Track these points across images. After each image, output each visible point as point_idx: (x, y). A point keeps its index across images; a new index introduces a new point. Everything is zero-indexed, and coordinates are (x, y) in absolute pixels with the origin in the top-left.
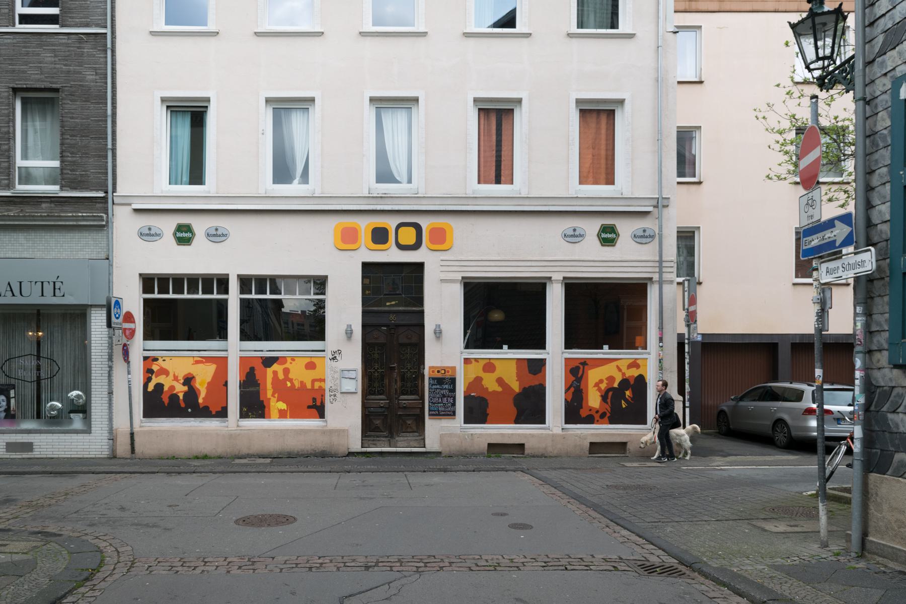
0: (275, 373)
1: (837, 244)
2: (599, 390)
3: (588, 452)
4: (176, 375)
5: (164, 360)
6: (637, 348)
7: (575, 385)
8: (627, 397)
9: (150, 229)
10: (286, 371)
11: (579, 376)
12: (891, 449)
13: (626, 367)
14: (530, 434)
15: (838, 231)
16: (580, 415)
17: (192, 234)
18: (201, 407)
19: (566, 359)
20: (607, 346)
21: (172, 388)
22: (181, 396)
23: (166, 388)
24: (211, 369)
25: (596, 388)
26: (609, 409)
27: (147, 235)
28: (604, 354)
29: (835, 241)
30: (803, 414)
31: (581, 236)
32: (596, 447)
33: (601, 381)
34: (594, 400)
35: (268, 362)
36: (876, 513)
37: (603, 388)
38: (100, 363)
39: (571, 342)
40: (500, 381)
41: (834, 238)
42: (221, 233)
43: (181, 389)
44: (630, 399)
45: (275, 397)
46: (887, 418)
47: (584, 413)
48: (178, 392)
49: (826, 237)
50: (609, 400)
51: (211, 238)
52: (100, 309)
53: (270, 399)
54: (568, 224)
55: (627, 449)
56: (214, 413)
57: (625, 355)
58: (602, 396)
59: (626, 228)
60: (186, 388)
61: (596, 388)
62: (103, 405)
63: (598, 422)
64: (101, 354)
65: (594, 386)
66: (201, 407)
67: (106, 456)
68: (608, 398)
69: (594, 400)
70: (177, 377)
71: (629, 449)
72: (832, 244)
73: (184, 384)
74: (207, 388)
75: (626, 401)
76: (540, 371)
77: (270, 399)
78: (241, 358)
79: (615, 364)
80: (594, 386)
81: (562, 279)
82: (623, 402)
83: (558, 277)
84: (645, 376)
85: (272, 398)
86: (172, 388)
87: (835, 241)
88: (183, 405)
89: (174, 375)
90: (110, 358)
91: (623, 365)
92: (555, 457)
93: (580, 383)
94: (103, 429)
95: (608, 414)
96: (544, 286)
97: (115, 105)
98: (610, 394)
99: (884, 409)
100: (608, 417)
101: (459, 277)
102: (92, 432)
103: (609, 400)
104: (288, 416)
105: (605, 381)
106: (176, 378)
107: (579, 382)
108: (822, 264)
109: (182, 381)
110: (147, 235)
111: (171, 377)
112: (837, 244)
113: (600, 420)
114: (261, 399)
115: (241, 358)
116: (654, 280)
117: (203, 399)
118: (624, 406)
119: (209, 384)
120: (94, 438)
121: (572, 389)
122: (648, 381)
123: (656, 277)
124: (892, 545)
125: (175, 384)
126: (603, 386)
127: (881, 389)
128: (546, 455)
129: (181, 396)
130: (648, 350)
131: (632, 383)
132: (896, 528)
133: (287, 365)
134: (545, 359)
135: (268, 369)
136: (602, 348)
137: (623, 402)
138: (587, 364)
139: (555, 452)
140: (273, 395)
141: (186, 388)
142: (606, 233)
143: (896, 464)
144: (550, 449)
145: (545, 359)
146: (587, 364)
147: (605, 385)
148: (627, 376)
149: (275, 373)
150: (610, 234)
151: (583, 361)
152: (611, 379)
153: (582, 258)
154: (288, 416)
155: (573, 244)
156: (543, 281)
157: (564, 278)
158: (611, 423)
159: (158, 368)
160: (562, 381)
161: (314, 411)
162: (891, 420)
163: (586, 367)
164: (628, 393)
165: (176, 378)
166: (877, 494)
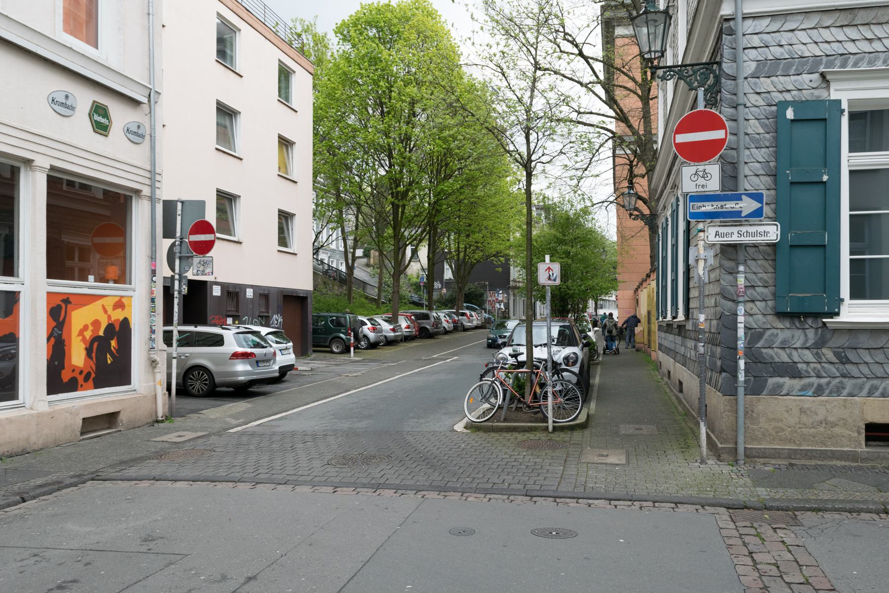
1: (743, 215)
2: (84, 340)
3: (79, 434)
6: (107, 281)
7: (56, 334)
8: (112, 348)
11: (61, 319)
13: (111, 307)
14: (7, 419)
15: (745, 205)
16: (62, 379)
17: (109, 122)
20: (93, 277)
25: (80, 338)
26: (94, 368)
27: (62, 104)
28: (90, 287)
29: (741, 212)
30: (230, 359)
31: (72, 108)
32: (91, 424)
33: (86, 327)
34: (78, 356)
36: (751, 426)
37: (88, 337)
39: (56, 269)
41: (740, 209)
44: (115, 352)
46: (762, 353)
47: (66, 376)
49: (727, 206)
50: (94, 355)
51: (130, 136)
54: (60, 85)
55: (119, 421)
57: (111, 290)
58: (86, 349)
59: (120, 115)
61: (80, 338)
63: (83, 388)
65: (78, 335)
68: (93, 352)
69: (78, 356)
71: (122, 421)
72: (738, 214)
75: (112, 354)
76: (11, 313)
78: (49, 293)
79: (100, 303)
80: (78, 335)
81: (49, 167)
82: (108, 356)
83: (43, 162)
84: (129, 319)
87: (741, 212)
91: (109, 303)
92: (41, 449)
93: (62, 331)
95: (93, 375)
96: (14, 172)
98: (96, 344)
99: (759, 345)
100: (94, 379)
103: (94, 355)
105: (91, 328)
107: (61, 329)
108: (710, 228)
112: (743, 215)
113: (84, 384)
115: (49, 293)
116: (143, 193)
118: (109, 362)
121: (53, 340)
122: (132, 326)
123: (146, 191)
124: (773, 447)
126: (88, 334)
127: (753, 330)
128: (29, 450)
130: (133, 286)
131: (117, 329)
132: (774, 434)
134: (19, 292)
136: (87, 280)
137: (108, 356)
138: (70, 302)
139: (40, 443)
142: (99, 116)
143: (771, 386)
144: (33, 439)
145: (19, 292)
146: (70, 302)
147: (91, 333)
148: (113, 319)
150: (103, 117)
151: (65, 297)
152: (96, 323)
153: (74, 143)
155: (61, 117)
156: (16, 164)
157: (53, 168)
158: (96, 386)
162: (766, 353)
163: (69, 306)
164: (113, 343)
166: (753, 411)
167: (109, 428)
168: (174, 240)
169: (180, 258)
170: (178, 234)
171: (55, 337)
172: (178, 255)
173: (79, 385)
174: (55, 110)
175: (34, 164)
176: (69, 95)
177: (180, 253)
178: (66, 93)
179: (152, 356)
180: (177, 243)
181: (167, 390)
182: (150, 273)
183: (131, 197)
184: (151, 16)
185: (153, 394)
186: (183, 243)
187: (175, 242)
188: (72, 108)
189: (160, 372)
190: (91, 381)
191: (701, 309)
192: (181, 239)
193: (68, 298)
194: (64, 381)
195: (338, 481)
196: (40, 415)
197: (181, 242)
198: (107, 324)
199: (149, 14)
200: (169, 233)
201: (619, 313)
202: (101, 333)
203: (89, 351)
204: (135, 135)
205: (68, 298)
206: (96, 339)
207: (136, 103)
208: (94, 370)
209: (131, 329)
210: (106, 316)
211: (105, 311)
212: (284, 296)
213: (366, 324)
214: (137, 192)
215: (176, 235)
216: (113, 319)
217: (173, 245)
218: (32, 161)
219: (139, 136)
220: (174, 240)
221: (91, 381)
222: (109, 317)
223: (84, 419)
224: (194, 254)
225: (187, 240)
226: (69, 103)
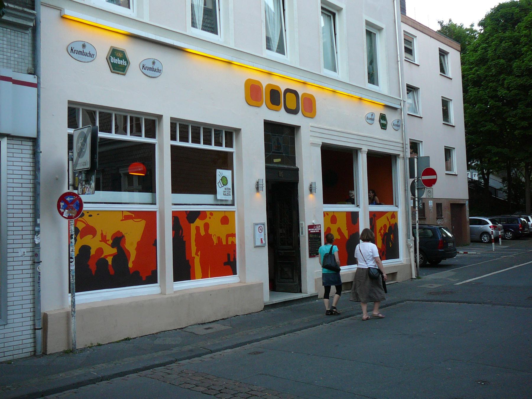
0: (198, 228)
4: (104, 234)
5: (90, 216)
9: (84, 46)
10: (207, 226)
12: (474, 146)
17: (127, 63)
18: (131, 272)
19: (370, 212)
21: (100, 251)
22: (110, 260)
23: (93, 252)
24: (140, 225)
27: (80, 53)
31: (159, 71)
35: (193, 216)
38: (20, 220)
40: (339, 230)
42: (157, 68)
43: (109, 251)
45: (198, 256)
48: (106, 256)
51: (146, 71)
52: (20, 142)
53: (194, 258)
56: (144, 279)
60: (114, 251)
62: (24, 280)
64: (22, 207)
65: (379, 233)
66: (131, 272)
67: (28, 355)
70: (105, 236)
73: (113, 246)
74: (137, 249)
77: (194, 258)
80: (379, 233)
83: (365, 149)
85: (196, 256)
86: (100, 251)
88: (112, 272)
89: (102, 234)
90: (36, 214)
94: (24, 315)
97: (269, 44)
101: (320, 142)
102: (9, 321)
104: (209, 276)
106: (104, 239)
109: (110, 242)
110: (80, 53)
111: (98, 237)
114: (187, 259)
117: (133, 262)
119: (139, 244)
120: (11, 330)
125: (103, 245)
129: (110, 260)
133: (207, 220)
135: (192, 224)
140: (197, 254)
141: (114, 251)
149: (198, 228)
152: (385, 226)
154: (209, 276)
159: (84, 225)
160: (184, 282)
161: (228, 267)
165: (104, 239)
167: (392, 280)
168: (414, 179)
169: (418, 189)
170: (416, 176)
172: (416, 187)
175: (362, 150)
176: (86, 44)
177: (418, 186)
178: (83, 43)
180: (416, 181)
181: (415, 262)
185: (410, 264)
186: (419, 180)
187: (415, 180)
188: (159, 71)
191: (72, 251)
192: (417, 178)
197: (418, 180)
200: (412, 176)
201: (433, 201)
202: (387, 231)
206: (385, 234)
207: (395, 109)
209: (398, 229)
211: (388, 220)
212: (451, 204)
213: (488, 224)
215: (415, 176)
216: (391, 224)
217: (414, 182)
219: (155, 71)
220: (414, 179)
222: (390, 223)
224: (425, 186)
225: (421, 179)
226: (155, 67)
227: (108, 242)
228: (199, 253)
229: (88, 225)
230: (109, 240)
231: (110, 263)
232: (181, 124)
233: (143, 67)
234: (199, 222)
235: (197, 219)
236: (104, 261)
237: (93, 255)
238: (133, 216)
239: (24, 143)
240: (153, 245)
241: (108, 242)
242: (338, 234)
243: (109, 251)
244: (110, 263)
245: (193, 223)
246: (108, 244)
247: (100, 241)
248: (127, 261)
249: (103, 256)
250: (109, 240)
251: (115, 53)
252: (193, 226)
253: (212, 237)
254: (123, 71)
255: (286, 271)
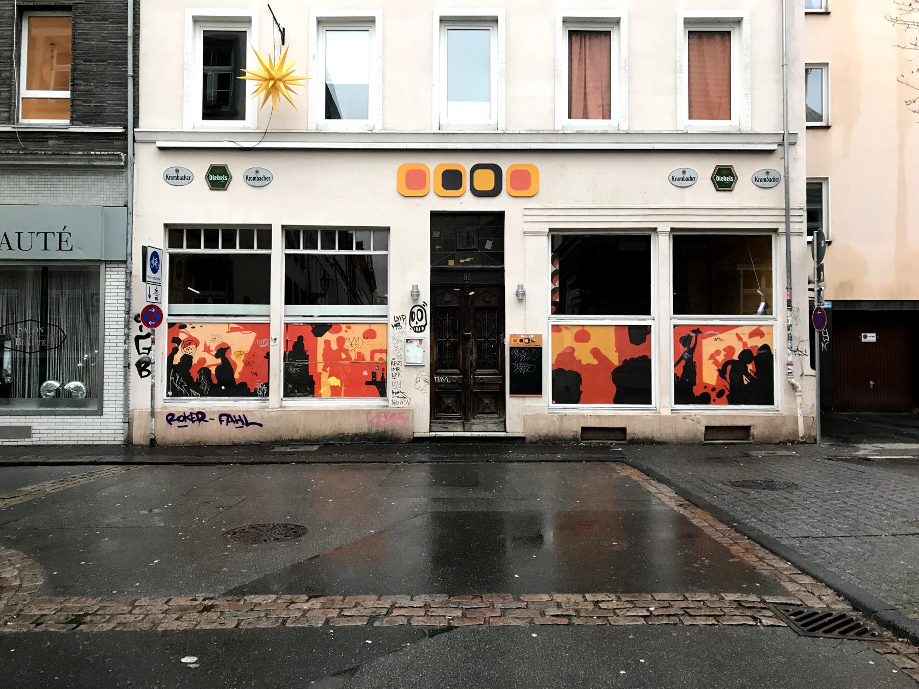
2: (716, 363)
8: (749, 371)
11: (691, 346)
16: (693, 394)
17: (228, 177)
18: (237, 383)
21: (203, 360)
22: (213, 370)
23: (195, 361)
25: (712, 361)
31: (692, 179)
33: (718, 352)
34: (709, 375)
43: (213, 362)
48: (210, 366)
50: (727, 376)
53: (321, 373)
54: (676, 165)
58: (719, 370)
60: (219, 361)
65: (710, 359)
66: (237, 383)
69: (709, 375)
70: (209, 347)
73: (217, 356)
75: (748, 376)
77: (321, 373)
82: (744, 377)
83: (664, 228)
85: (324, 373)
86: (203, 360)
89: (205, 345)
91: (745, 333)
95: (727, 393)
96: (648, 238)
98: (729, 367)
100: (727, 396)
103: (727, 376)
106: (207, 349)
111: (201, 347)
114: (310, 374)
117: (240, 373)
118: (746, 383)
120: (106, 420)
122: (774, 353)
123: (782, 228)
125: (206, 355)
126: (721, 358)
129: (213, 370)
130: (774, 315)
135: (319, 338)
137: (744, 377)
141: (219, 361)
145: (651, 326)
146: (701, 332)
148: (749, 346)
149: (327, 343)
151: (695, 328)
152: (730, 350)
155: (682, 189)
156: (647, 233)
158: (730, 403)
163: (699, 335)
164: (750, 367)
165: (207, 349)
171: (685, 360)
173: (712, 400)
174: (677, 186)
176: (259, 169)
178: (175, 169)
179: (790, 380)
182: (786, 303)
183: (771, 236)
184: (785, 66)
188: (692, 179)
189: (800, 396)
190: (724, 398)
193: (698, 329)
194: (696, 395)
195: (347, 598)
196: (661, 417)
198: (741, 350)
199: (783, 66)
202: (736, 357)
203: (722, 373)
204: (765, 181)
205: (698, 329)
208: (729, 388)
210: (741, 343)
214: (775, 230)
218: (656, 228)
219: (687, 180)
221: (724, 398)
223: (707, 428)
227: (212, 353)
228: (328, 369)
229: (190, 336)
230: (212, 351)
231: (213, 372)
232: (260, 230)
233: (673, 178)
234: (328, 336)
235: (327, 332)
236: (207, 371)
237: (195, 364)
238: (241, 327)
239: (120, 266)
240: (265, 357)
241: (212, 353)
242: (592, 357)
243: (213, 362)
244: (213, 372)
245: (321, 336)
246: (212, 355)
247: (203, 351)
248: (232, 372)
249: (205, 366)
250: (212, 351)
251: (215, 170)
252: (321, 341)
253: (349, 352)
254: (811, 187)
255: (487, 404)
